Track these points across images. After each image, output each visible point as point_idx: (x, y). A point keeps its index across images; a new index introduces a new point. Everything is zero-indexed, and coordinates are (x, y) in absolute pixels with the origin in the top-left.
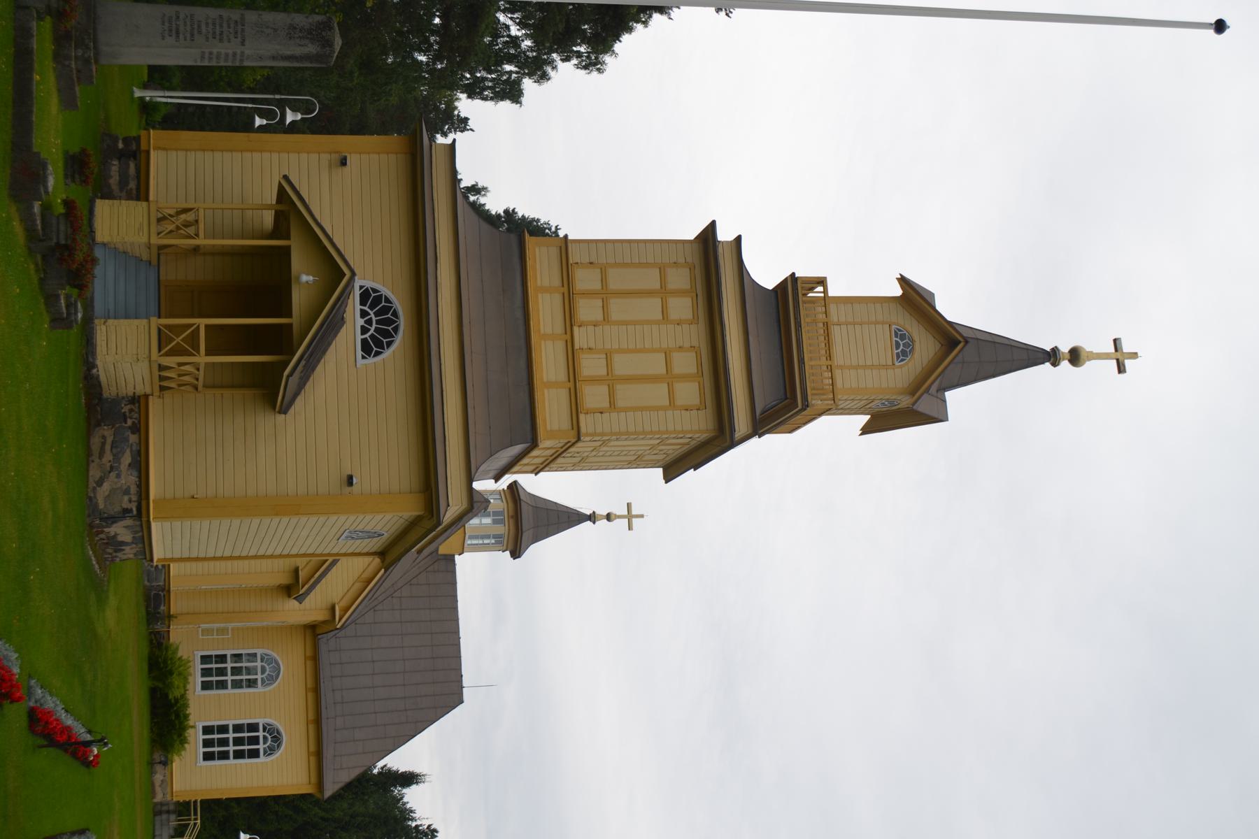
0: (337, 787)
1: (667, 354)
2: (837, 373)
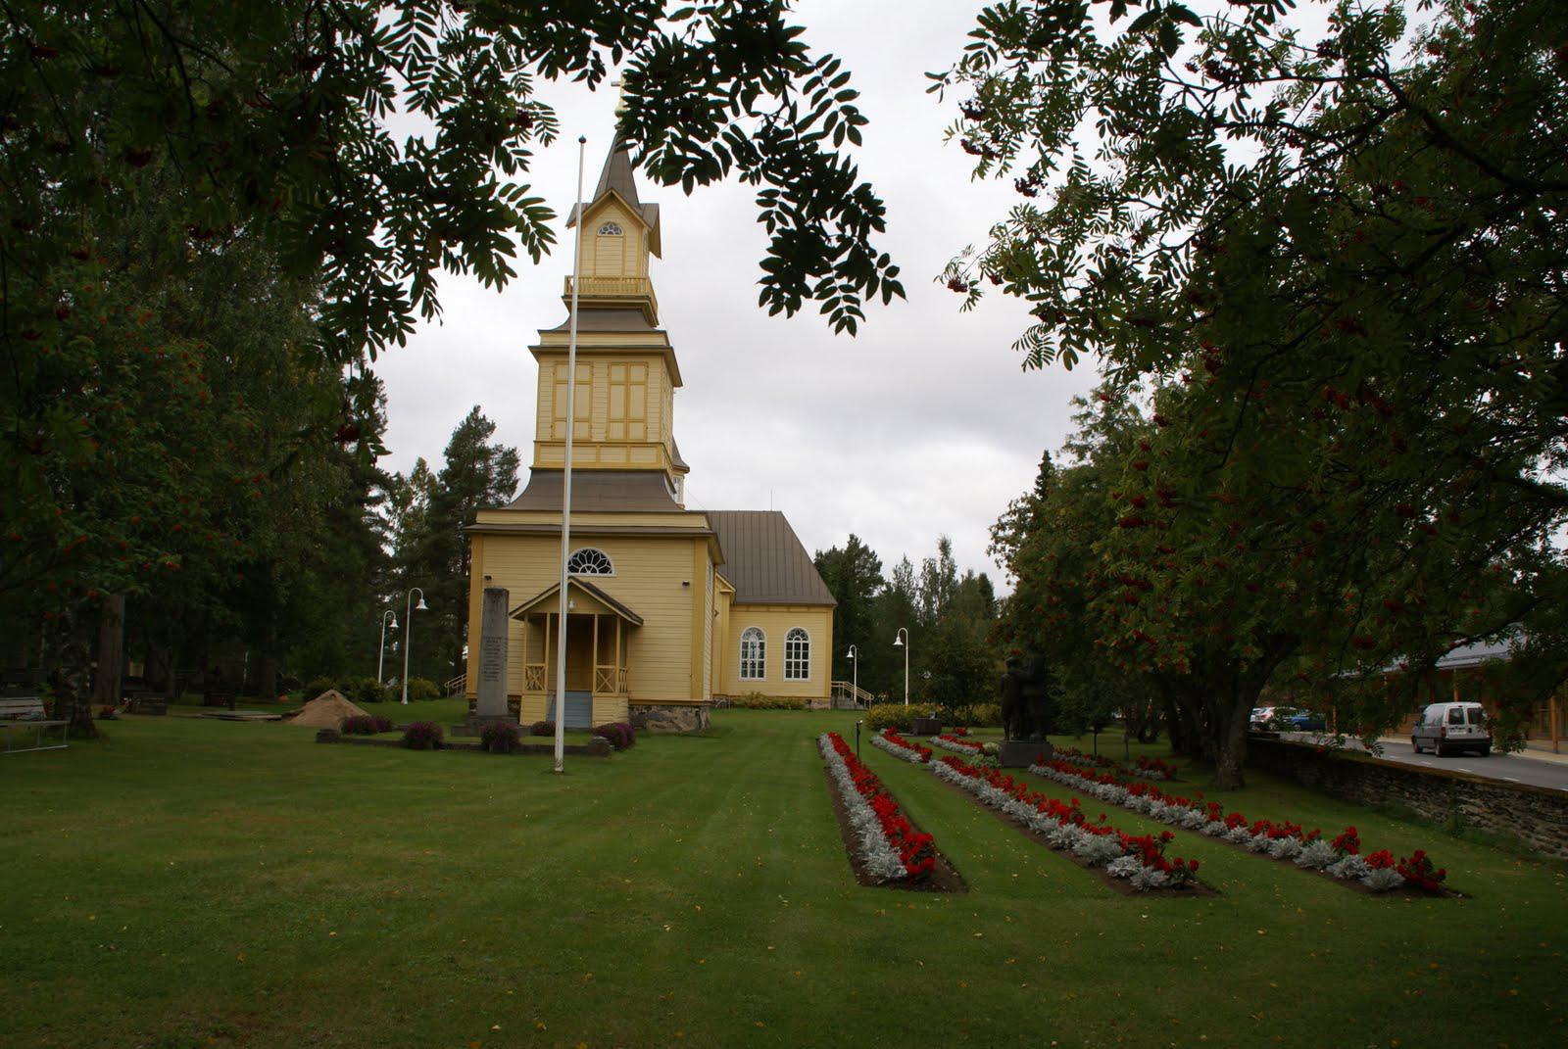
0: (830, 595)
1: (611, 384)
2: (628, 274)
